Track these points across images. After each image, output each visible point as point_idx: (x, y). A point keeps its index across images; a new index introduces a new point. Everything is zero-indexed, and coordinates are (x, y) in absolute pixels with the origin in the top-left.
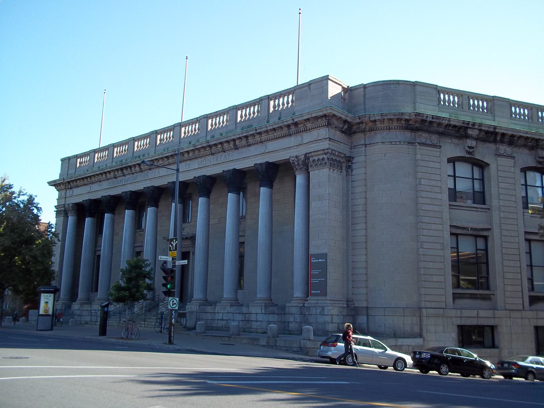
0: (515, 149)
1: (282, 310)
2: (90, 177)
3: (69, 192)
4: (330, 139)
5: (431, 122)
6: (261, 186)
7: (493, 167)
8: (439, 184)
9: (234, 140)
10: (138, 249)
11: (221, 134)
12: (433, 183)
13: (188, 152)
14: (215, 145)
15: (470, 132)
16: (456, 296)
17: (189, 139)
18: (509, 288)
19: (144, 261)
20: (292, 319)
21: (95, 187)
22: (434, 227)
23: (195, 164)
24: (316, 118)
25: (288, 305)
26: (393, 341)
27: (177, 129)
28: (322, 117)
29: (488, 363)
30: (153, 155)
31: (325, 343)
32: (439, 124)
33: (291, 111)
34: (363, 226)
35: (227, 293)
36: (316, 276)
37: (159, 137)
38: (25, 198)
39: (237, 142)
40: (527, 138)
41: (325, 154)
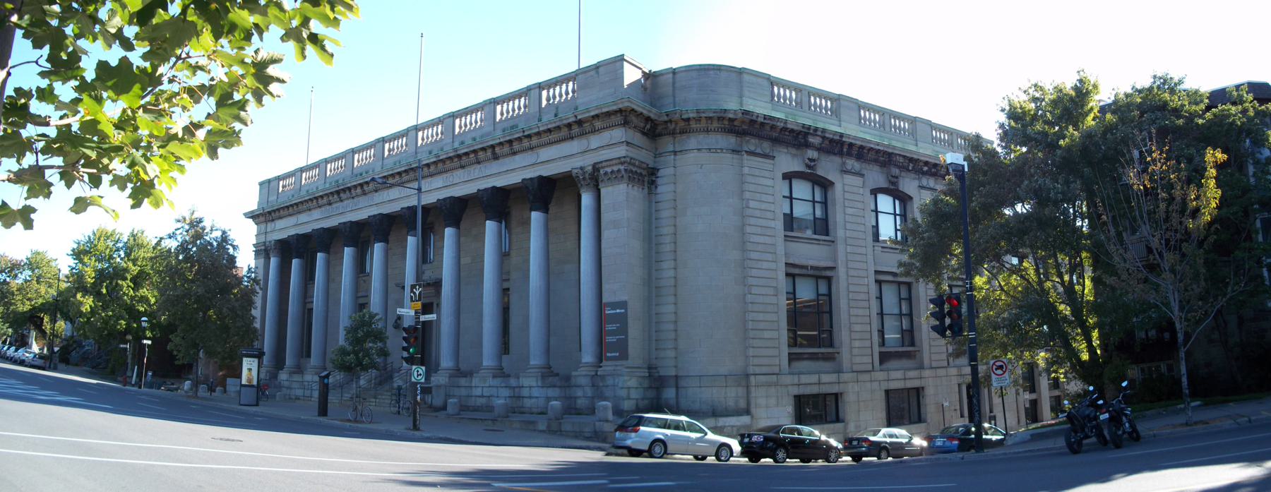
0: (864, 165)
1: (566, 381)
2: (297, 204)
3: (270, 226)
4: (628, 143)
5: (762, 124)
6: (531, 210)
7: (838, 187)
8: (772, 207)
9: (493, 147)
10: (362, 301)
11: (474, 139)
12: (764, 206)
13: (428, 165)
14: (466, 154)
15: (811, 139)
16: (793, 358)
17: (429, 149)
18: (857, 344)
19: (372, 316)
20: (579, 393)
21: (303, 218)
22: (765, 265)
23: (438, 182)
24: (608, 114)
25: (574, 373)
26: (712, 421)
27: (412, 133)
28: (615, 112)
29: (834, 443)
30: (379, 173)
31: (622, 428)
32: (773, 127)
33: (572, 104)
34: (670, 264)
35: (488, 358)
36: (612, 333)
37: (387, 146)
38: (218, 234)
39: (497, 149)
40: (878, 151)
41: (622, 163)
